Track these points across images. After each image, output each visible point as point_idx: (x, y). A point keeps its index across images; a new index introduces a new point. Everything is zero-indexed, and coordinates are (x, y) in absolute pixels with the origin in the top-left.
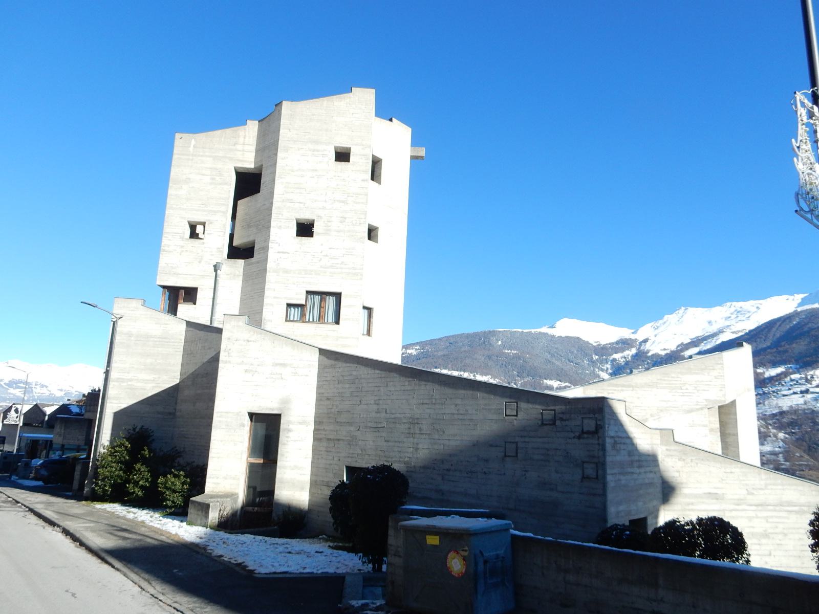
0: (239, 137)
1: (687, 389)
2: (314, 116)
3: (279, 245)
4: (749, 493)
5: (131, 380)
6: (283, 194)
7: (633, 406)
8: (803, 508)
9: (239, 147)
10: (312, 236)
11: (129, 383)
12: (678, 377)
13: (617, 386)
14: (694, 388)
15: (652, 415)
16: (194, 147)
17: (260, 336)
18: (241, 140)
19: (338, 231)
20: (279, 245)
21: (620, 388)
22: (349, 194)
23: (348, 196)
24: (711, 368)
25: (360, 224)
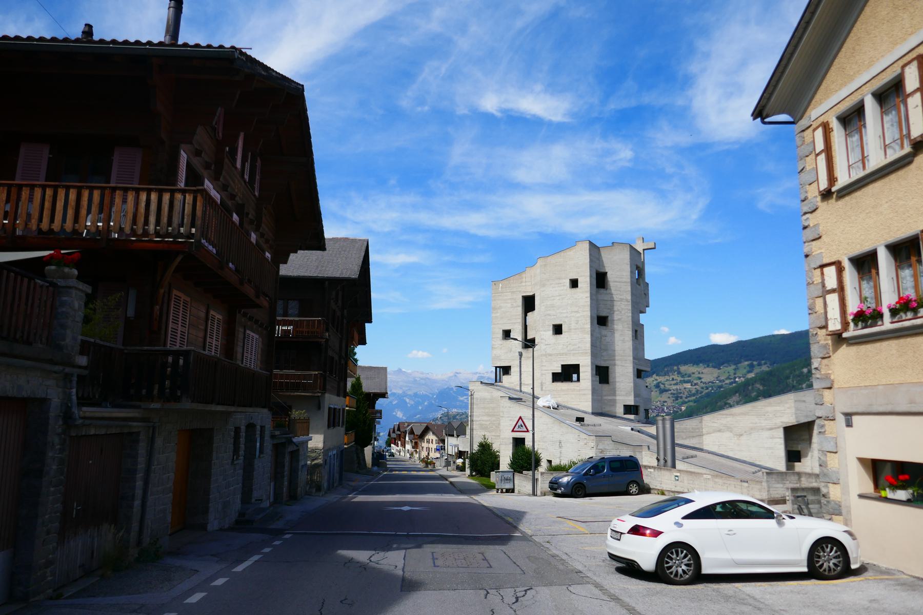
5: (480, 421)
9: (524, 284)
10: (561, 334)
13: (723, 415)
15: (745, 432)
18: (524, 280)
19: (575, 329)
21: (724, 416)
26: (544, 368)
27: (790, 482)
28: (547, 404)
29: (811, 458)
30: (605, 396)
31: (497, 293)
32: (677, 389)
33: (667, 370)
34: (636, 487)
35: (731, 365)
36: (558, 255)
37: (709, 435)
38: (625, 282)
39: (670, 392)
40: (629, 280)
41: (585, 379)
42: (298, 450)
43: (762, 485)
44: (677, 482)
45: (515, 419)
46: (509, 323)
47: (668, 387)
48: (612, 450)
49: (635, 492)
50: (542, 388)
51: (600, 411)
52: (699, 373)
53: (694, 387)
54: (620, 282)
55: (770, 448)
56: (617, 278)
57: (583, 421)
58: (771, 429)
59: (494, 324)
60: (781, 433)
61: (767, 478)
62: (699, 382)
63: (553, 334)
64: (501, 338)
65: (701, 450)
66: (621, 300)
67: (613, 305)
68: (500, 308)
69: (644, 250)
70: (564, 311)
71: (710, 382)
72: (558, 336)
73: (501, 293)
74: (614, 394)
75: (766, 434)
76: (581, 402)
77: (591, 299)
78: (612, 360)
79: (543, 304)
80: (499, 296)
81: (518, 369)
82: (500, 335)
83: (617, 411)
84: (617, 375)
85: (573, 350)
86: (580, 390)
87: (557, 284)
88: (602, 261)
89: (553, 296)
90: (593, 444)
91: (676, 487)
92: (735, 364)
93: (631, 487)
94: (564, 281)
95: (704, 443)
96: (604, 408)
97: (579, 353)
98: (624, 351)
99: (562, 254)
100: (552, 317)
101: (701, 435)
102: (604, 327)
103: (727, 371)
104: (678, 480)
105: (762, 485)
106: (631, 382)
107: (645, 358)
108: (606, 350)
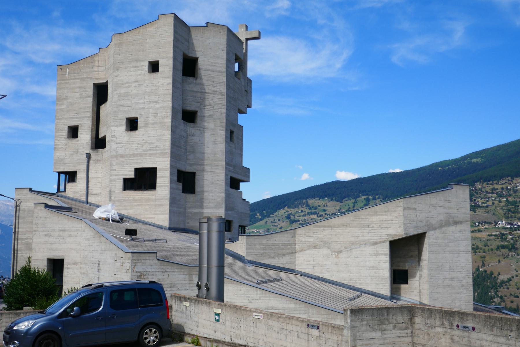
0: (95, 62)
1: (373, 227)
3: (117, 138)
4: (250, 302)
5: (27, 239)
6: (118, 102)
7: (332, 241)
8: (280, 311)
9: (96, 69)
11: (26, 241)
12: (366, 218)
13: (320, 227)
14: (378, 226)
15: (345, 248)
16: (69, 74)
17: (51, 214)
18: (97, 63)
19: (153, 124)
20: (117, 138)
21: (322, 229)
22: (160, 95)
23: (159, 97)
24: (393, 210)
25: (167, 116)
26: (114, 173)
27: (395, 327)
28: (104, 216)
29: (420, 279)
30: (190, 208)
31: (63, 80)
32: (305, 220)
33: (297, 203)
34: (155, 332)
35: (351, 199)
36: (136, 31)
37: (302, 252)
38: (220, 72)
39: (299, 223)
40: (224, 70)
41: (162, 186)
43: (342, 335)
44: (218, 325)
45: (146, 249)
46: (77, 118)
47: (297, 218)
48: (157, 273)
49: (154, 341)
50: (110, 198)
51: (182, 226)
52: (324, 206)
53: (320, 218)
54: (213, 71)
55: (374, 268)
56: (209, 65)
57: (136, 235)
58: (375, 244)
59: (59, 119)
60: (386, 249)
61: (351, 321)
62: (323, 213)
63: (127, 130)
64: (66, 136)
65: (292, 271)
66: (214, 92)
67: (205, 98)
68: (66, 98)
69: (247, 40)
70: (142, 101)
71: (333, 214)
72: (133, 133)
73: (68, 80)
74: (202, 207)
75: (370, 249)
77: (173, 86)
78: (199, 165)
79: (115, 93)
80: (66, 83)
82: (65, 132)
84: (206, 182)
85: (150, 150)
86: (156, 200)
87: (133, 67)
88: (193, 43)
89: (128, 83)
90: (128, 265)
91: (215, 332)
92: (354, 198)
93: (146, 333)
94: (142, 63)
95: (297, 262)
96: (188, 223)
97: (155, 154)
99: (141, 30)
100: (126, 109)
101: (293, 253)
102: (192, 125)
103: (348, 204)
104: (218, 321)
105: (342, 335)
106: (222, 192)
107: (243, 165)
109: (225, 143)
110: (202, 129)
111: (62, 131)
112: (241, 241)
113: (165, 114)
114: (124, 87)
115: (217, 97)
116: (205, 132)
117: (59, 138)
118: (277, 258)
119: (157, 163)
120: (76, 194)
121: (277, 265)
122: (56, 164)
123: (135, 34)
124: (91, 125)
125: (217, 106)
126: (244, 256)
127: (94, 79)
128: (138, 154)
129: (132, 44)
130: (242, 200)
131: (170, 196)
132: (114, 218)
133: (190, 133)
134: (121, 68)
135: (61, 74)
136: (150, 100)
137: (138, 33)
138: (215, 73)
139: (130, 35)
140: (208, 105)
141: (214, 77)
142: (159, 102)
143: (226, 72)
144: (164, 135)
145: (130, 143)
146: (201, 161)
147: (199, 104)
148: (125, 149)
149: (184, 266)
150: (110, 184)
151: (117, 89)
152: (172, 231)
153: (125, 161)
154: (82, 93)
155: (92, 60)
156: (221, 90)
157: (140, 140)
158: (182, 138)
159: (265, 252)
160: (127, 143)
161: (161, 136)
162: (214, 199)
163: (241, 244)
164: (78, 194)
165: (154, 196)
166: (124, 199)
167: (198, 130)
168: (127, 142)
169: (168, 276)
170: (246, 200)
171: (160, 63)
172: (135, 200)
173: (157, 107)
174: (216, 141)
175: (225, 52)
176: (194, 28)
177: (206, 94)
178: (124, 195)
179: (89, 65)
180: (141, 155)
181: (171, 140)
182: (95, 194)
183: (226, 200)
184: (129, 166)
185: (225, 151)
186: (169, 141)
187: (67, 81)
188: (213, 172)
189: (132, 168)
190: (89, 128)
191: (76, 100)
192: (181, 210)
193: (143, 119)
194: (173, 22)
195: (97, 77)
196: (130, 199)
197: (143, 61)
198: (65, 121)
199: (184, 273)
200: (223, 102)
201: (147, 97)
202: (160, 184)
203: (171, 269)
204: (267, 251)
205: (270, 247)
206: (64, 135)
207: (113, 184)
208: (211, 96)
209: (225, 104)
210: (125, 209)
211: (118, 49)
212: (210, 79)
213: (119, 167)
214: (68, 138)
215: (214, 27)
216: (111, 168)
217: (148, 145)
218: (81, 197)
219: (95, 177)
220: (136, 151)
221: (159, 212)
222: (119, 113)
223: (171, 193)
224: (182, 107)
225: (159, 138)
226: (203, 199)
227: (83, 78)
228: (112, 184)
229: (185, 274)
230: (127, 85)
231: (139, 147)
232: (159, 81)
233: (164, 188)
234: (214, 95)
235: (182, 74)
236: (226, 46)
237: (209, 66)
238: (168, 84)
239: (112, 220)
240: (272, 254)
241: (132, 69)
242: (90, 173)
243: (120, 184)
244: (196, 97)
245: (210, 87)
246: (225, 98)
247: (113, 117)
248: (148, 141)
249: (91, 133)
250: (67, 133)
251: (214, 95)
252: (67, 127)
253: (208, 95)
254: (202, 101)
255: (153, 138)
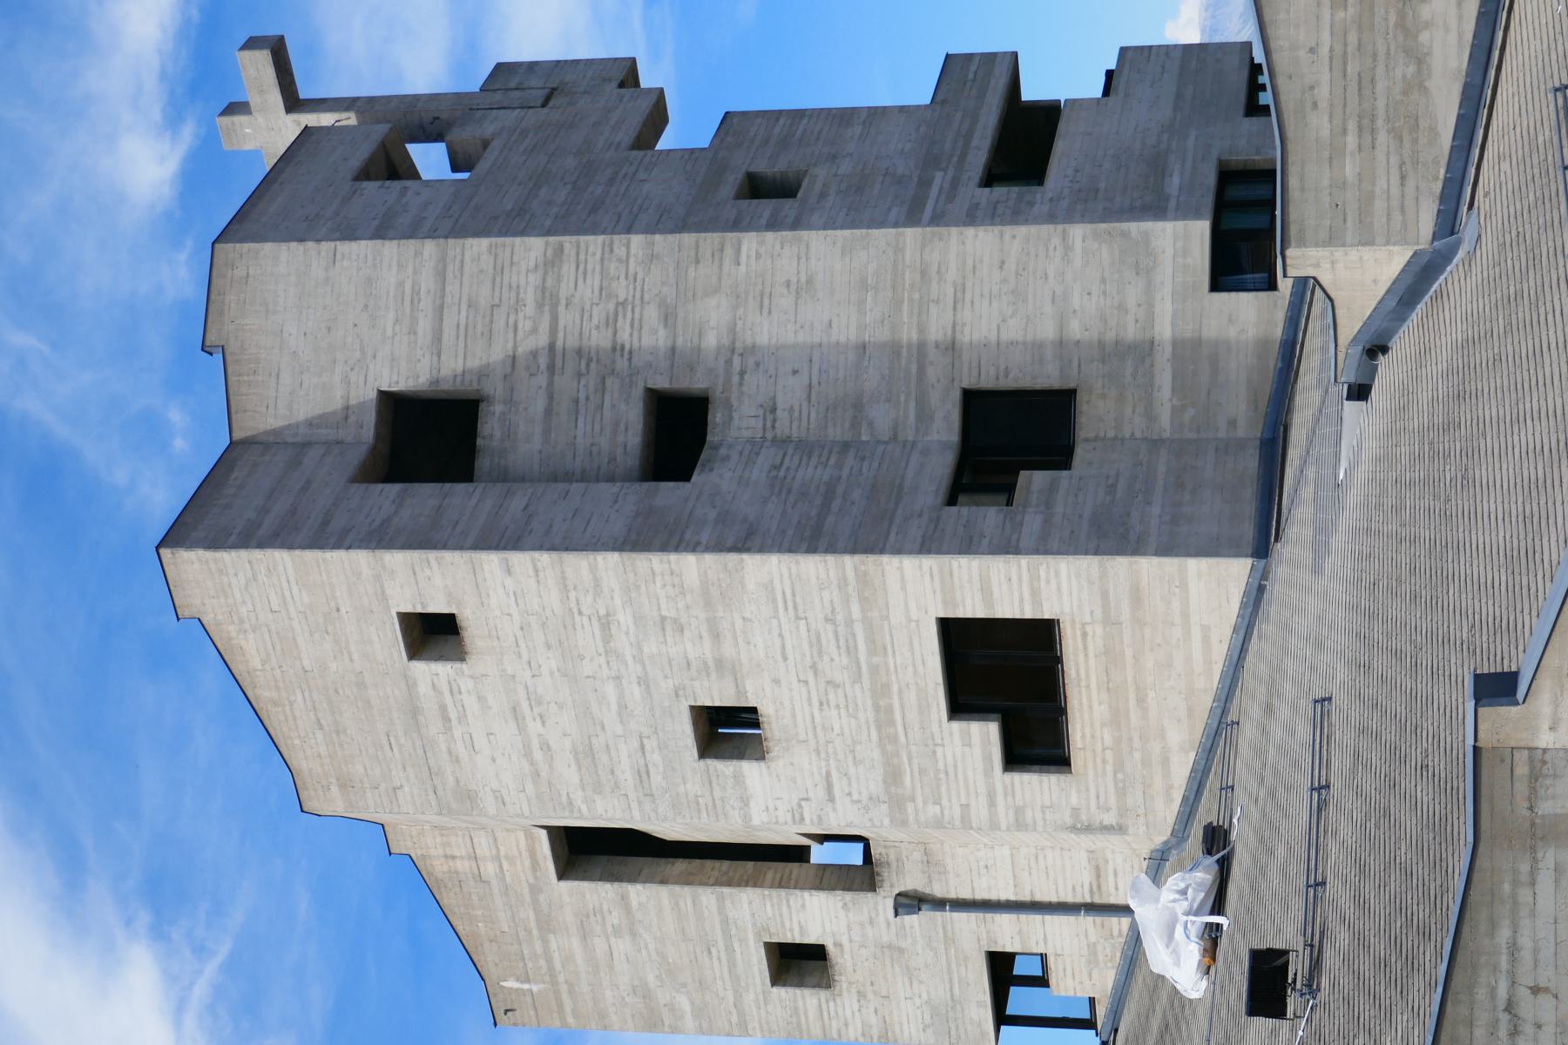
0: (457, 872)
2: (323, 722)
3: (806, 799)
9: (489, 869)
18: (463, 866)
19: (716, 636)
23: (580, 613)
26: (980, 812)
28: (1192, 952)
30: (1150, 416)
31: (560, 1005)
38: (441, 275)
40: (429, 247)
42: (1518, 704)
46: (730, 950)
50: (1106, 829)
51: (1251, 462)
54: (440, 310)
56: (413, 332)
66: (548, 299)
67: (579, 352)
69: (293, 103)
74: (1143, 351)
76: (1186, 616)
78: (921, 370)
79: (584, 808)
80: (571, 992)
81: (1005, 920)
83: (1252, 333)
84: (1013, 331)
85: (851, 650)
86: (1110, 621)
87: (448, 729)
88: (310, 423)
89: (527, 753)
94: (423, 688)
96: (1233, 423)
97: (868, 625)
98: (864, 286)
99: (263, 694)
100: (655, 757)
102: (716, 417)
107: (927, 100)
108: (859, 406)
109: (804, 234)
110: (737, 361)
111: (796, 1008)
112: (1317, 265)
113: (658, 585)
114: (551, 767)
115: (572, 285)
116: (749, 341)
117: (834, 1023)
118: (1424, 37)
119: (914, 614)
120: (1101, 957)
121: (1469, 36)
122: (959, 1037)
123: (287, 720)
124: (758, 891)
125: (614, 284)
126: (1411, 254)
127: (536, 878)
128: (877, 708)
129: (338, 732)
130: (1111, 99)
131: (1086, 553)
132: (1202, 895)
133: (760, 425)
134: (457, 781)
135: (532, 1013)
136: (601, 650)
137: (280, 709)
138: (448, 299)
139: (297, 742)
140: (615, 334)
141: (469, 306)
142: (602, 612)
143: (442, 241)
144: (769, 587)
145: (822, 741)
146: (904, 362)
147: (609, 382)
148: (856, 763)
149: (1476, 877)
150: (1040, 828)
151: (564, 799)
152: (1277, 540)
153: (915, 761)
154: (610, 929)
155: (450, 885)
156: (532, 264)
157: (805, 696)
158: (782, 473)
159: (1388, 120)
160: (823, 755)
161: (774, 601)
162: (1103, 281)
163: (1340, 266)
164: (1099, 948)
165: (1089, 629)
166: (1109, 768)
167: (741, 384)
168: (818, 752)
169: (1541, 997)
170: (1113, 66)
171: (408, 608)
172: (1117, 718)
173: (630, 621)
174: (794, 279)
175: (345, 247)
176: (234, 417)
177: (559, 343)
178: (1090, 764)
179: (474, 897)
180: (881, 691)
181: (790, 551)
182: (1098, 876)
183: (1109, 215)
184: (943, 745)
185: (847, 232)
186: (798, 563)
187: (564, 988)
188: (960, 289)
189: (951, 734)
190: (770, 896)
191: (644, 953)
192: (1162, 468)
193: (697, 684)
194: (201, 553)
195: (527, 863)
196: (1108, 741)
197: (411, 685)
198: (752, 996)
199: (1524, 878)
200: (591, 249)
201: (587, 668)
202: (1022, 600)
203: (1495, 969)
204: (1381, 104)
205: (1353, 88)
206: (815, 1001)
207: (1039, 816)
208: (566, 318)
209: (601, 238)
210: (1165, 762)
211: (369, 795)
212: (479, 328)
213: (948, 790)
214: (828, 986)
215: (221, 314)
216: (958, 823)
217: (826, 658)
218: (1116, 933)
219: (1010, 874)
220: (861, 715)
221: (1176, 605)
222: (681, 789)
223: (1071, 547)
224: (627, 478)
225: (786, 609)
226: (1101, 345)
227: (538, 920)
228: (1040, 822)
229: (1533, 871)
230: (538, 755)
231: (842, 700)
232: (497, 613)
233: (1043, 584)
234: (563, 302)
235: (461, 488)
236: (310, 244)
237: (415, 333)
238: (509, 571)
239: (1212, 913)
240: (1399, 73)
241: (457, 733)
242: (993, 896)
243: (1034, 785)
244: (577, 401)
245: (520, 325)
246: (574, 238)
247: (704, 815)
248: (808, 658)
249: (798, 892)
250: (807, 992)
251: (563, 302)
252: (775, 990)
253: (561, 335)
254: (593, 365)
255: (787, 635)
